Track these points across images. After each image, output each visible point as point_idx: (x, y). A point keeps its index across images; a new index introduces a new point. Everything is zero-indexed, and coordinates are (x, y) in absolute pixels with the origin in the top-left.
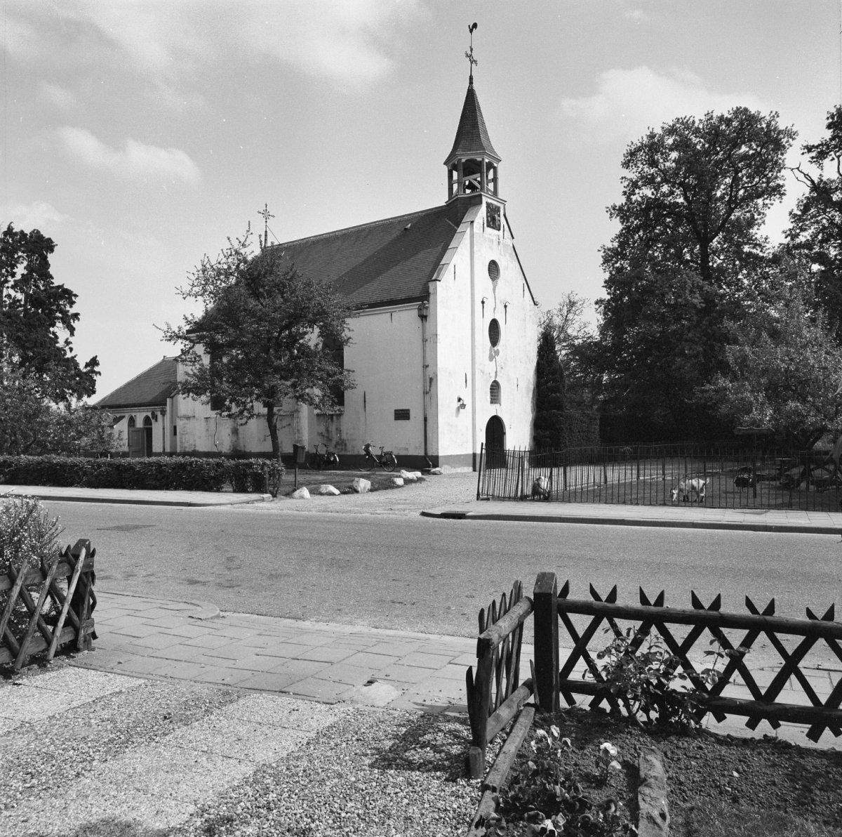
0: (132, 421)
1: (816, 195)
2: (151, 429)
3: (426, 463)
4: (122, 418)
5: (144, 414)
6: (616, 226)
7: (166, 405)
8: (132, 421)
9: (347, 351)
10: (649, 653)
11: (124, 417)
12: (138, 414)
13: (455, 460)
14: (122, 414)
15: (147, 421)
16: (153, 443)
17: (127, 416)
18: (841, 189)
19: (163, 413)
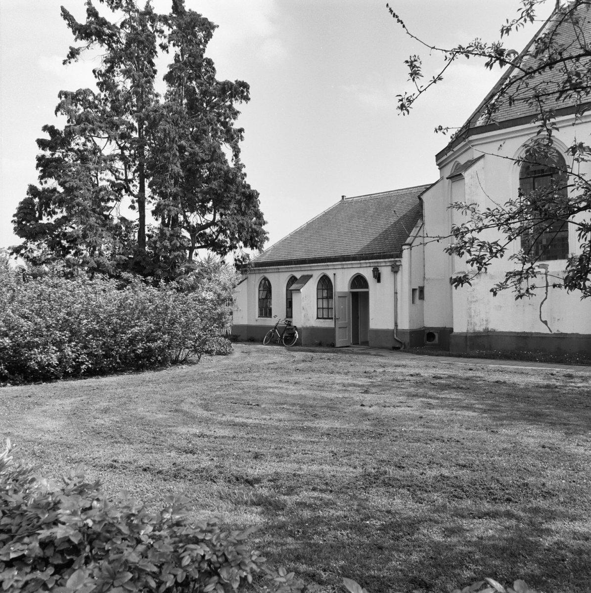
0: (325, 283)
1: (93, 19)
2: (366, 295)
3: (98, 548)
4: (306, 279)
5: (353, 272)
6: (168, 70)
7: (400, 256)
8: (325, 283)
9: (240, 154)
10: (193, 139)
11: (309, 277)
12: (339, 273)
13: (44, 553)
14: (309, 273)
15: (359, 281)
16: (507, 330)
17: (317, 275)
18: (590, 87)
19: (395, 269)
